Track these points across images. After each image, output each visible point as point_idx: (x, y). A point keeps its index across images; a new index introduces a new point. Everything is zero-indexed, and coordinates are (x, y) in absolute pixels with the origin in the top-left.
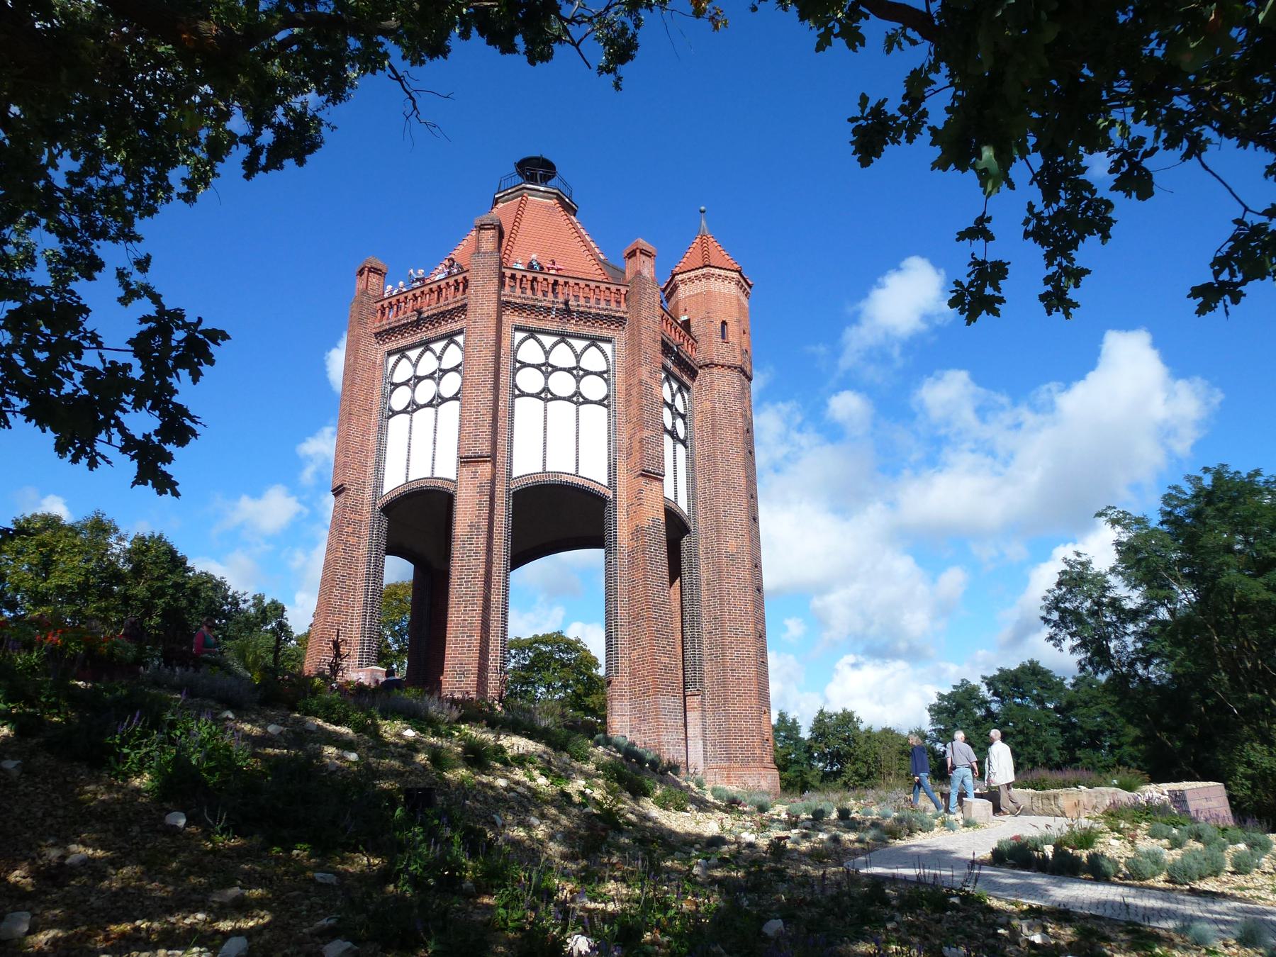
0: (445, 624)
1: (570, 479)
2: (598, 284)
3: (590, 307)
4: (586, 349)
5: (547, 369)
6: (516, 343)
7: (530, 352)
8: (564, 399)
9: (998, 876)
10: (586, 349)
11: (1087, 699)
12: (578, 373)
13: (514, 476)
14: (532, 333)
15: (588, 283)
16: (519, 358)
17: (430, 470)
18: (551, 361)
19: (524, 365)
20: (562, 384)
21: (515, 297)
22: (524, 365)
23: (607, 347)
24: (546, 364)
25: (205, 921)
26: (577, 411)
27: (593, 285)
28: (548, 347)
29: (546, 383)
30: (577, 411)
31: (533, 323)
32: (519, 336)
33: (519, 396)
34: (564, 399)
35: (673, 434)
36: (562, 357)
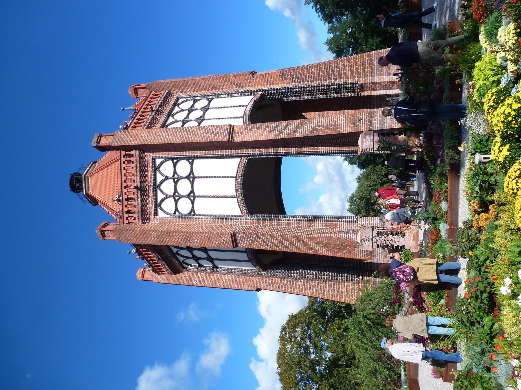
0: (325, 256)
1: (240, 199)
2: (124, 206)
3: (136, 167)
4: (162, 174)
5: (176, 197)
6: (164, 215)
7: (168, 206)
8: (192, 167)
9: (445, 17)
10: (162, 174)
11: (346, 347)
12: (176, 179)
13: (240, 214)
14: (157, 205)
15: (123, 175)
16: (173, 212)
17: (239, 119)
18: (171, 175)
19: (176, 209)
20: (184, 187)
21: (137, 179)
22: (176, 209)
23: (158, 162)
24: (174, 196)
25: (485, 27)
26: (199, 197)
27: (124, 172)
28: (164, 196)
29: (184, 178)
30: (199, 197)
31: (152, 205)
32: (160, 213)
33: (194, 212)
34: (192, 167)
35: (206, 109)
36: (168, 187)
